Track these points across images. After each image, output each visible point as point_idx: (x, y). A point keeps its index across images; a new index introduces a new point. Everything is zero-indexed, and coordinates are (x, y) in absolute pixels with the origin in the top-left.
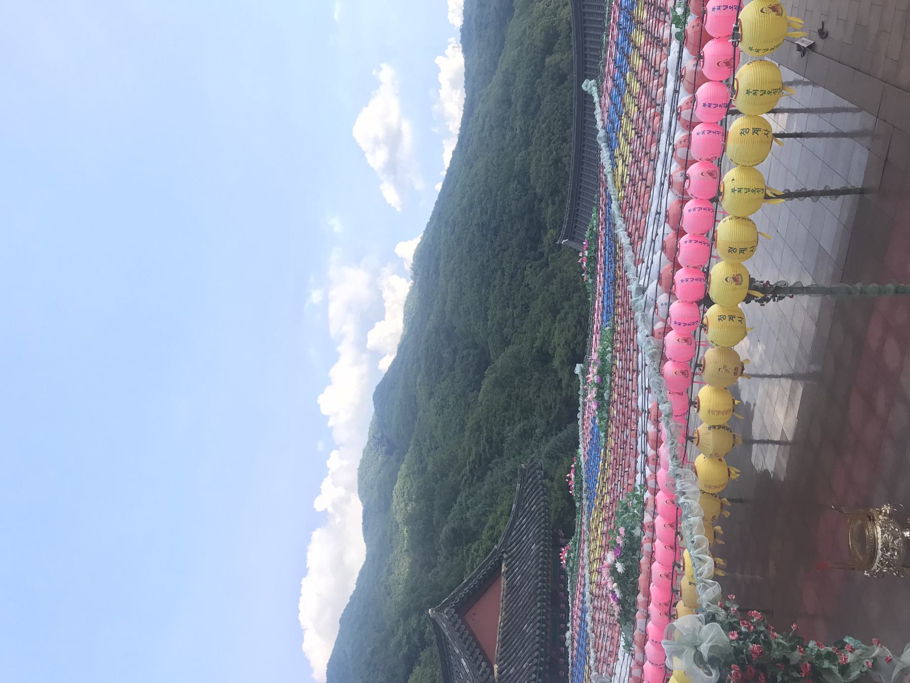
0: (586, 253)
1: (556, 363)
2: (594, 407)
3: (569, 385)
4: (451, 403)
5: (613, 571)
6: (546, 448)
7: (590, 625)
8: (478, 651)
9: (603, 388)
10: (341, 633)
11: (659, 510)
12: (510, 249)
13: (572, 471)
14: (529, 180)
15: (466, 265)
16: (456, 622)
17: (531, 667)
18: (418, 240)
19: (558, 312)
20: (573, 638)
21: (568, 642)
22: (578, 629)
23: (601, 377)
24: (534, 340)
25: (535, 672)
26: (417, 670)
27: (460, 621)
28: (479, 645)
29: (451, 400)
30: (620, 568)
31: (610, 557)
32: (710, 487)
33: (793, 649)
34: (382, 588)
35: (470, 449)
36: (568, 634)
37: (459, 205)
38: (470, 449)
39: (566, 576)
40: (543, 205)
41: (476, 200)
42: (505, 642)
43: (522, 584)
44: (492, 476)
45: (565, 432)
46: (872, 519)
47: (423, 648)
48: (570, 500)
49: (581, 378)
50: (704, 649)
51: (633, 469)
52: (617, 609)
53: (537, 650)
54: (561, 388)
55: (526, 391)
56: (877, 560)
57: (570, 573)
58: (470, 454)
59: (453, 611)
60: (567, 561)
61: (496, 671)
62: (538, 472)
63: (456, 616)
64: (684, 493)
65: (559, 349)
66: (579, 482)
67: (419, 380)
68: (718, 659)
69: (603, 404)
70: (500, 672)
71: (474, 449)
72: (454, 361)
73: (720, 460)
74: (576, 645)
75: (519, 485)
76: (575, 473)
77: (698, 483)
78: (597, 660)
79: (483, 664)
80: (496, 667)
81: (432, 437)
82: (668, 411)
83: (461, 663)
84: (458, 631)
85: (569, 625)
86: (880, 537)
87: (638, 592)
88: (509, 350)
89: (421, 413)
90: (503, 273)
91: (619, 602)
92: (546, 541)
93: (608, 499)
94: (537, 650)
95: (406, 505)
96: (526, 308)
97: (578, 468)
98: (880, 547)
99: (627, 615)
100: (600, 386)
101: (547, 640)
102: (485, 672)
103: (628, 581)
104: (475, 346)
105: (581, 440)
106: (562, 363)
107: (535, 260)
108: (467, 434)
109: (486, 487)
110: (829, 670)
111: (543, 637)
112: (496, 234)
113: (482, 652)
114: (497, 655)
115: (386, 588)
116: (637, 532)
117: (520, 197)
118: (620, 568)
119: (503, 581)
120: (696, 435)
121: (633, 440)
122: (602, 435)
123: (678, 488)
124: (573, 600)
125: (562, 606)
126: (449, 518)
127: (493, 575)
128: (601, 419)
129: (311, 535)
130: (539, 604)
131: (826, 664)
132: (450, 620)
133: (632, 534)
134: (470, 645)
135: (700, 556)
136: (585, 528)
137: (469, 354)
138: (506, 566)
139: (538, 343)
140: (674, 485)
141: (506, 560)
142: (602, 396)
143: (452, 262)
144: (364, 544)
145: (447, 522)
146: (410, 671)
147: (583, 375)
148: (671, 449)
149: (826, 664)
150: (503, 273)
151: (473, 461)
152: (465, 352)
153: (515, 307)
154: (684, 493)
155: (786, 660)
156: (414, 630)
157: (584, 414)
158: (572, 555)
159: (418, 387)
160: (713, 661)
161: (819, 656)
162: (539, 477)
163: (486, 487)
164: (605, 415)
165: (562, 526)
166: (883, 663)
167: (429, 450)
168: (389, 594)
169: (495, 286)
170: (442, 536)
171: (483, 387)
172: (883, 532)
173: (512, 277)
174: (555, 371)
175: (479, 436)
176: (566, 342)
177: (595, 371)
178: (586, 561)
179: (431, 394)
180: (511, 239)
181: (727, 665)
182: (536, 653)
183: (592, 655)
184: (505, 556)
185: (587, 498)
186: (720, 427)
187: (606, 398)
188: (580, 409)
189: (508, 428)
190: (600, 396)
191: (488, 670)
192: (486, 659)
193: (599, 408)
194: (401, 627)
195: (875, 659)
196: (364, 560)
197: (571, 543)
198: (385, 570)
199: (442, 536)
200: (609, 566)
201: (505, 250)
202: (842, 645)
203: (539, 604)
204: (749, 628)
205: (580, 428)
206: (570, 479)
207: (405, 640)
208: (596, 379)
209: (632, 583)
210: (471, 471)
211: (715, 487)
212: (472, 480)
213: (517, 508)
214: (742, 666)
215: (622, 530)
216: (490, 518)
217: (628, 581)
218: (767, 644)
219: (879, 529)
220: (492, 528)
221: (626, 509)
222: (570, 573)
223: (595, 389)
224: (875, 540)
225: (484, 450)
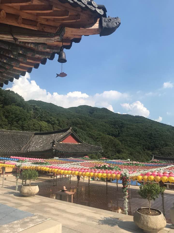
0: (156, 161)
3: (112, 158)
10: (48, 103)
12: (145, 142)
14: (165, 146)
15: (140, 130)
18: (113, 111)
19: (131, 155)
21: (71, 158)
26: (47, 123)
29: (104, 128)
30: (107, 167)
34: (59, 113)
36: (72, 158)
37: (157, 128)
39: (83, 157)
40: (158, 150)
41: (159, 132)
42: (66, 144)
49: (127, 160)
52: (98, 166)
54: (111, 156)
55: (110, 147)
59: (72, 133)
63: (70, 134)
67: (109, 119)
75: (97, 146)
89: (101, 120)
90: (139, 140)
91: (100, 167)
96: (130, 147)
104: (119, 134)
105: (116, 160)
107: (143, 149)
112: (149, 138)
114: (64, 143)
117: (160, 144)
119: (77, 143)
127: (78, 141)
129: (146, 108)
137: (116, 132)
139: (122, 150)
143: (141, 127)
144: (68, 108)
146: (46, 122)
150: (139, 140)
153: (130, 144)
156: (55, 122)
158: (87, 159)
159: (107, 119)
168: (57, 114)
169: (135, 138)
173: (138, 143)
175: (98, 136)
180: (148, 142)
191: (61, 141)
198: (63, 113)
201: (145, 140)
206: (104, 158)
207: (52, 120)
225: (95, 137)
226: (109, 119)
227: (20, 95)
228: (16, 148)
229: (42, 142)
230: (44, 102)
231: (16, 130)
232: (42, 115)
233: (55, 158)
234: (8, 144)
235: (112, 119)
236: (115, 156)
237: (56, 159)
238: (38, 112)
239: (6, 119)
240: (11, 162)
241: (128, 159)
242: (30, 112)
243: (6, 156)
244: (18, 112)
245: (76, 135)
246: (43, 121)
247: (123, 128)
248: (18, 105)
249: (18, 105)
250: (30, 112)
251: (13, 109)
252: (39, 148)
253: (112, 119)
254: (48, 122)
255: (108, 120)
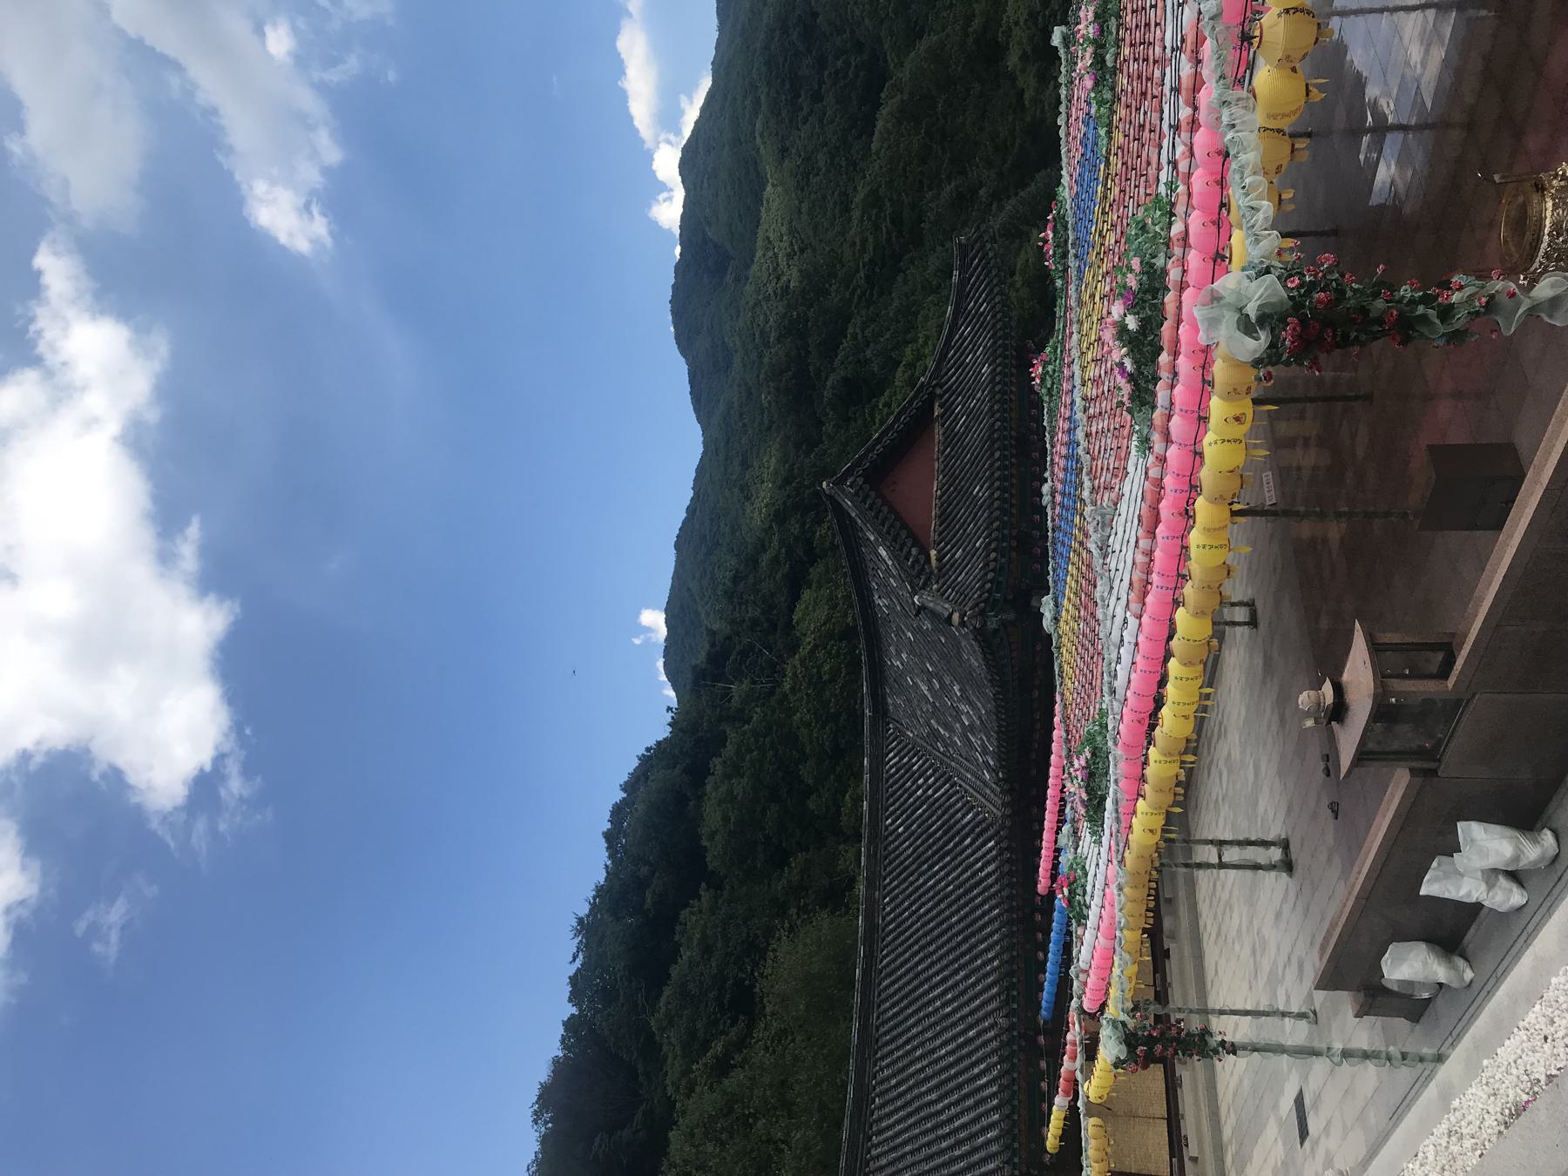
1: (1013, 60)
2: (1089, 83)
4: (821, 164)
5: (1122, 329)
6: (996, 223)
7: (1084, 444)
8: (904, 534)
9: (1103, 46)
10: (680, 563)
11: (1194, 201)
13: (1050, 226)
16: (867, 496)
17: (989, 544)
20: (1053, 493)
21: (1046, 499)
22: (1061, 475)
23: (1101, 27)
24: (969, 19)
25: (994, 550)
26: (807, 595)
27: (873, 494)
28: (904, 526)
29: (822, 159)
30: (1132, 323)
31: (1117, 310)
32: (1274, 117)
33: (1376, 295)
35: (864, 241)
36: (1046, 489)
38: (864, 241)
42: (943, 517)
43: (968, 428)
44: (905, 282)
45: (1032, 188)
46: (1540, 188)
47: (812, 563)
48: (1044, 277)
49: (1062, 53)
50: (1252, 310)
51: (1154, 165)
52: (1127, 388)
53: (997, 519)
56: (1541, 253)
57: (1046, 399)
58: (864, 249)
59: (860, 481)
60: (1043, 380)
61: (933, 558)
62: (988, 246)
63: (867, 487)
64: (1233, 126)
65: (1017, 31)
66: (1061, 244)
67: (759, 125)
68: (1270, 316)
69: (1103, 72)
70: (939, 559)
71: (871, 239)
72: (821, 83)
73: (1294, 70)
74: (1058, 498)
76: (1055, 231)
77: (1259, 109)
78: (1093, 490)
79: (914, 551)
80: (933, 553)
81: (792, 232)
82: (1214, 11)
83: (878, 555)
84: (871, 508)
85: (1047, 474)
86: (1549, 214)
87: (1162, 349)
88: (922, 46)
91: (1131, 378)
92: (1006, 357)
93: (1111, 239)
94: (997, 519)
95: (761, 356)
97: (1061, 221)
98: (1547, 230)
99: (1142, 396)
100: (1099, 46)
101: (1012, 506)
102: (917, 561)
103: (1144, 344)
106: (1024, 57)
108: (856, 214)
109: (896, 303)
110: (1424, 317)
111: (1004, 501)
113: (911, 534)
114: (933, 536)
115: (742, 490)
116: (1159, 262)
118: (1132, 323)
119: (938, 432)
120: (1257, 33)
121: (1156, 116)
122: (1102, 132)
123: (1225, 119)
124: (1052, 438)
125: (1036, 455)
126: (837, 363)
128: (1101, 103)
130: (997, 454)
131: (1421, 309)
132: (857, 494)
133: (1152, 266)
134: (892, 526)
135: (1253, 204)
136: (1073, 303)
138: (941, 406)
139: (976, 23)
140: (1218, 119)
141: (941, 396)
142: (1104, 61)
145: (834, 370)
146: (795, 597)
147: (1067, 46)
148: (1217, 66)
149: (1421, 309)
151: (871, 261)
152: (839, 63)
154: (1233, 126)
155: (1364, 311)
157: (1069, 116)
158: (1050, 368)
159: (758, 140)
160: (1263, 319)
161: (1413, 302)
162: (991, 254)
163: (896, 303)
164: (1108, 95)
165: (1034, 319)
166: (1504, 299)
167: (790, 256)
170: (827, 394)
171: (880, 124)
172: (1555, 207)
174: (1012, 78)
176: (1030, 14)
177: (1091, 16)
178: (1075, 353)
179: (784, 152)
181: (1283, 320)
182: (996, 524)
183: (1087, 484)
184: (938, 391)
185: (1076, 256)
186: (1296, 10)
187: (1109, 64)
188: (1062, 108)
189: (929, 195)
190: (1099, 61)
192: (916, 542)
193: (1096, 84)
194: (776, 538)
195: (1492, 297)
196: (701, 449)
197: (1048, 350)
199: (827, 394)
200: (1115, 324)
202: (1446, 285)
203: (997, 454)
204: (1315, 276)
205: (1062, 142)
206: (1045, 241)
208: (1091, 31)
209: (1151, 343)
210: (867, 277)
211: (1284, 115)
212: (872, 295)
213: (956, 313)
214: (1303, 322)
215: (1136, 263)
216: (908, 351)
217: (1144, 344)
218: (1340, 292)
219: (1550, 204)
220: (911, 366)
221: (1143, 228)
222: (1046, 399)
223: (1090, 50)
224: (1541, 220)
226: (759, 125)
227: (636, 763)
228: (980, 853)
229: (930, 682)
230: (691, 510)
231: (858, 800)
232: (755, 623)
233: (1047, 623)
234: (954, 908)
235: (757, 101)
236: (1028, 82)
237: (1056, 619)
238: (738, 648)
239: (789, 865)
240: (1082, 965)
241: (1056, 40)
242: (735, 702)
243: (1041, 955)
244: (741, 786)
245: (879, 440)
246: (795, 618)
247: (815, 15)
248: (698, 774)
249: (698, 774)
250: (735, 702)
251: (726, 819)
252: (971, 704)
253: (757, 101)
254: (796, 583)
255: (762, 136)
